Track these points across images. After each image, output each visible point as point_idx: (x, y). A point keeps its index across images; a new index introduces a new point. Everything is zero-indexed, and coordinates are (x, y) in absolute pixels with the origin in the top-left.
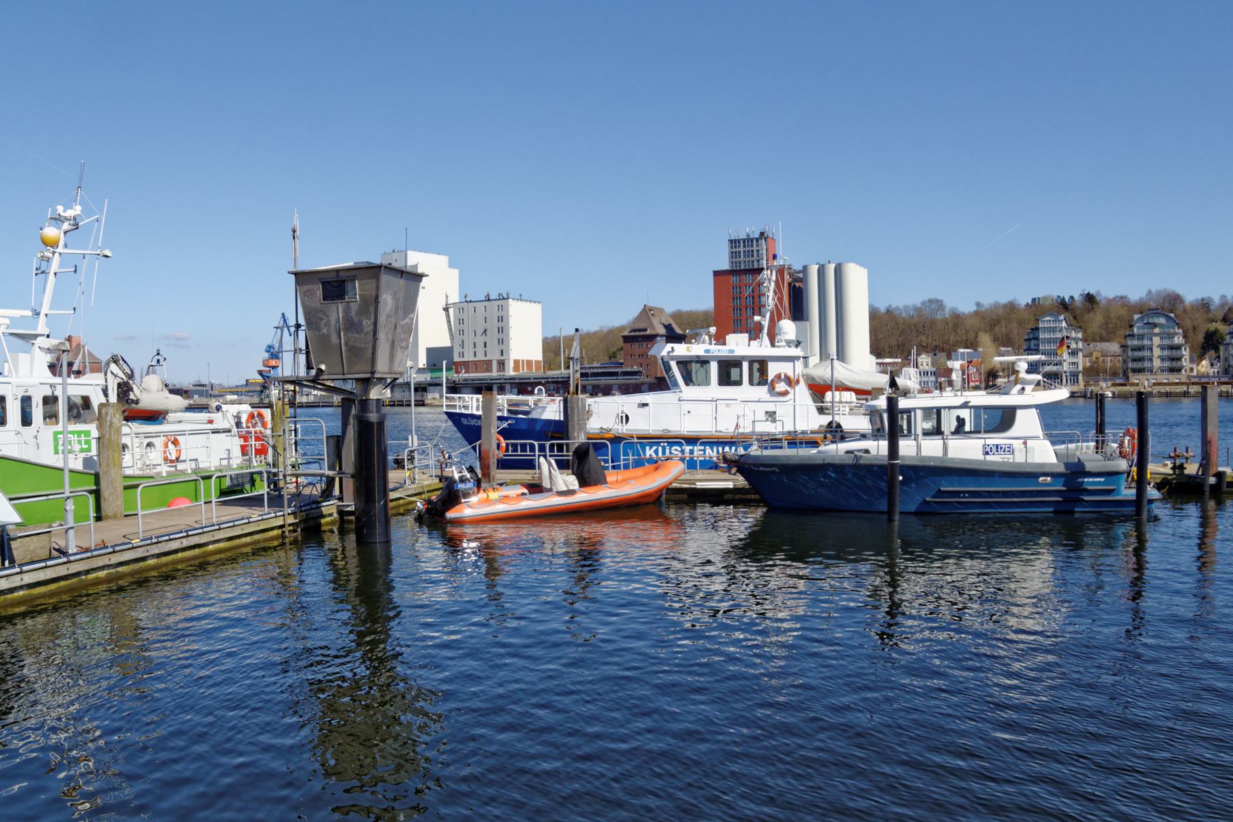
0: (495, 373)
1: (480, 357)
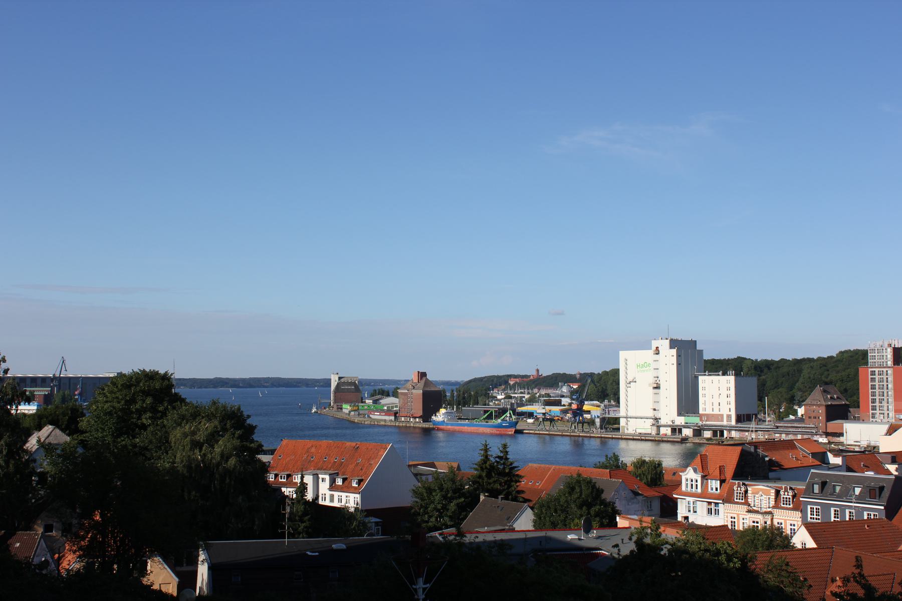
0: (725, 423)
1: (716, 412)
